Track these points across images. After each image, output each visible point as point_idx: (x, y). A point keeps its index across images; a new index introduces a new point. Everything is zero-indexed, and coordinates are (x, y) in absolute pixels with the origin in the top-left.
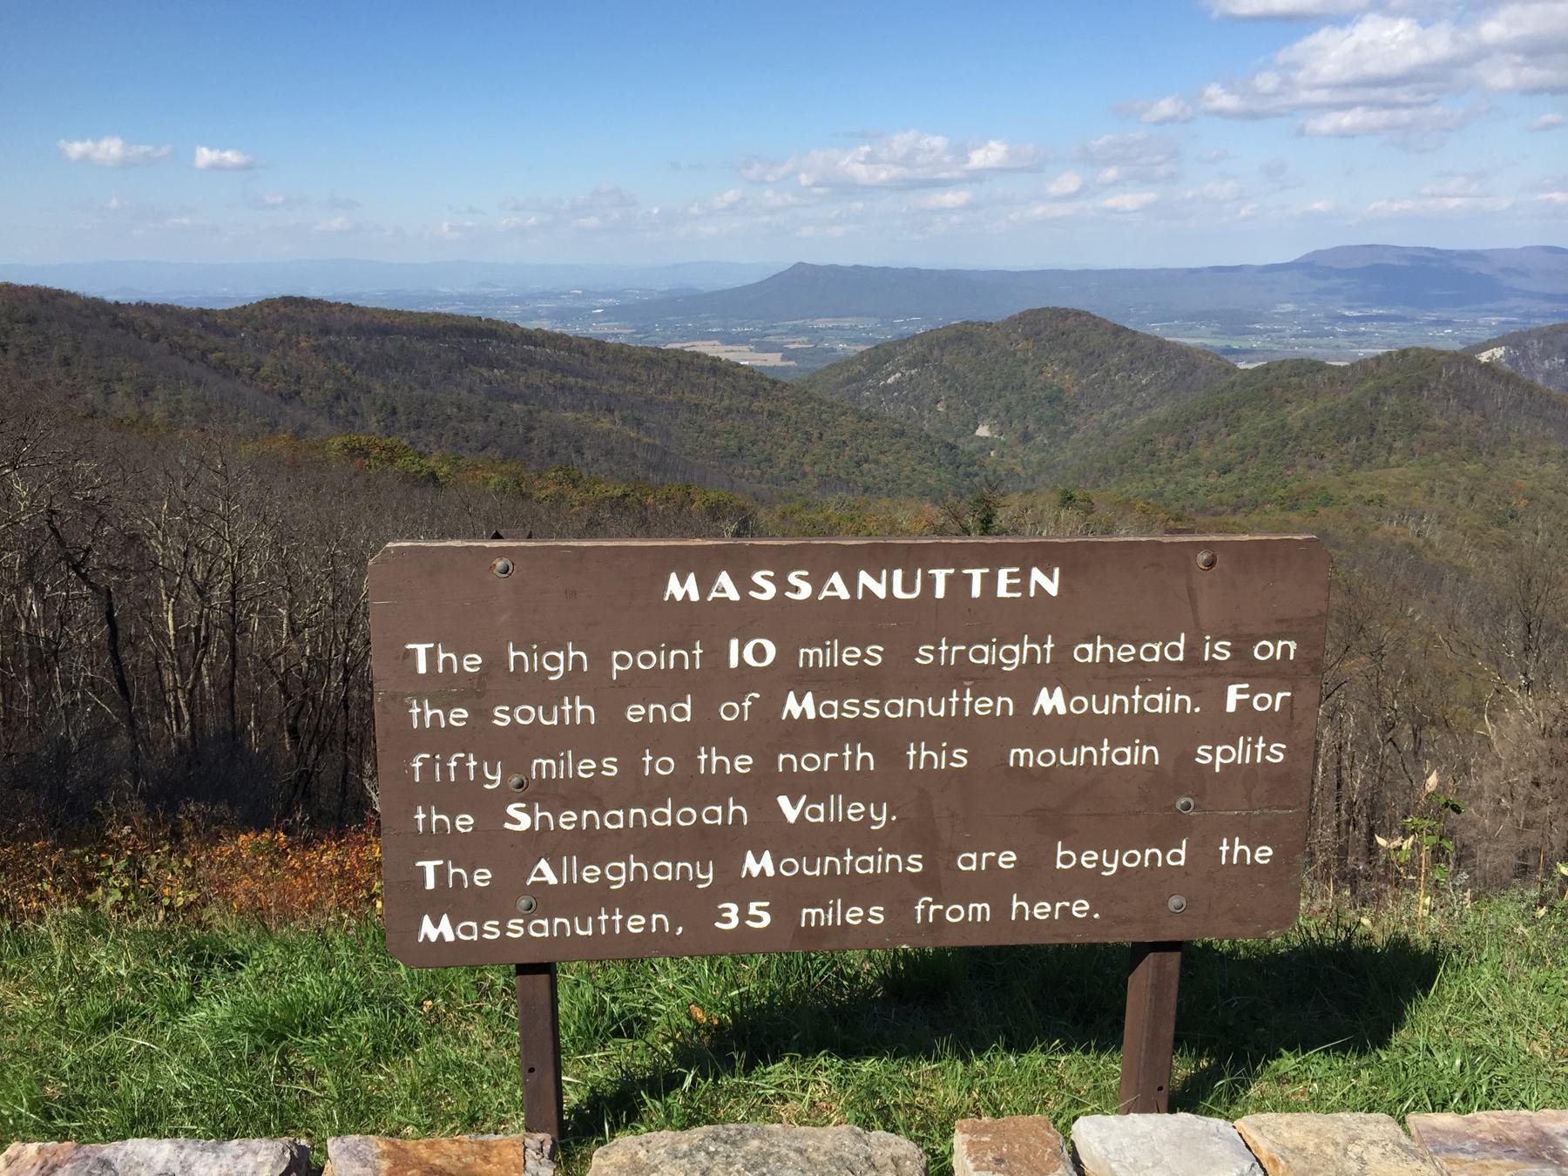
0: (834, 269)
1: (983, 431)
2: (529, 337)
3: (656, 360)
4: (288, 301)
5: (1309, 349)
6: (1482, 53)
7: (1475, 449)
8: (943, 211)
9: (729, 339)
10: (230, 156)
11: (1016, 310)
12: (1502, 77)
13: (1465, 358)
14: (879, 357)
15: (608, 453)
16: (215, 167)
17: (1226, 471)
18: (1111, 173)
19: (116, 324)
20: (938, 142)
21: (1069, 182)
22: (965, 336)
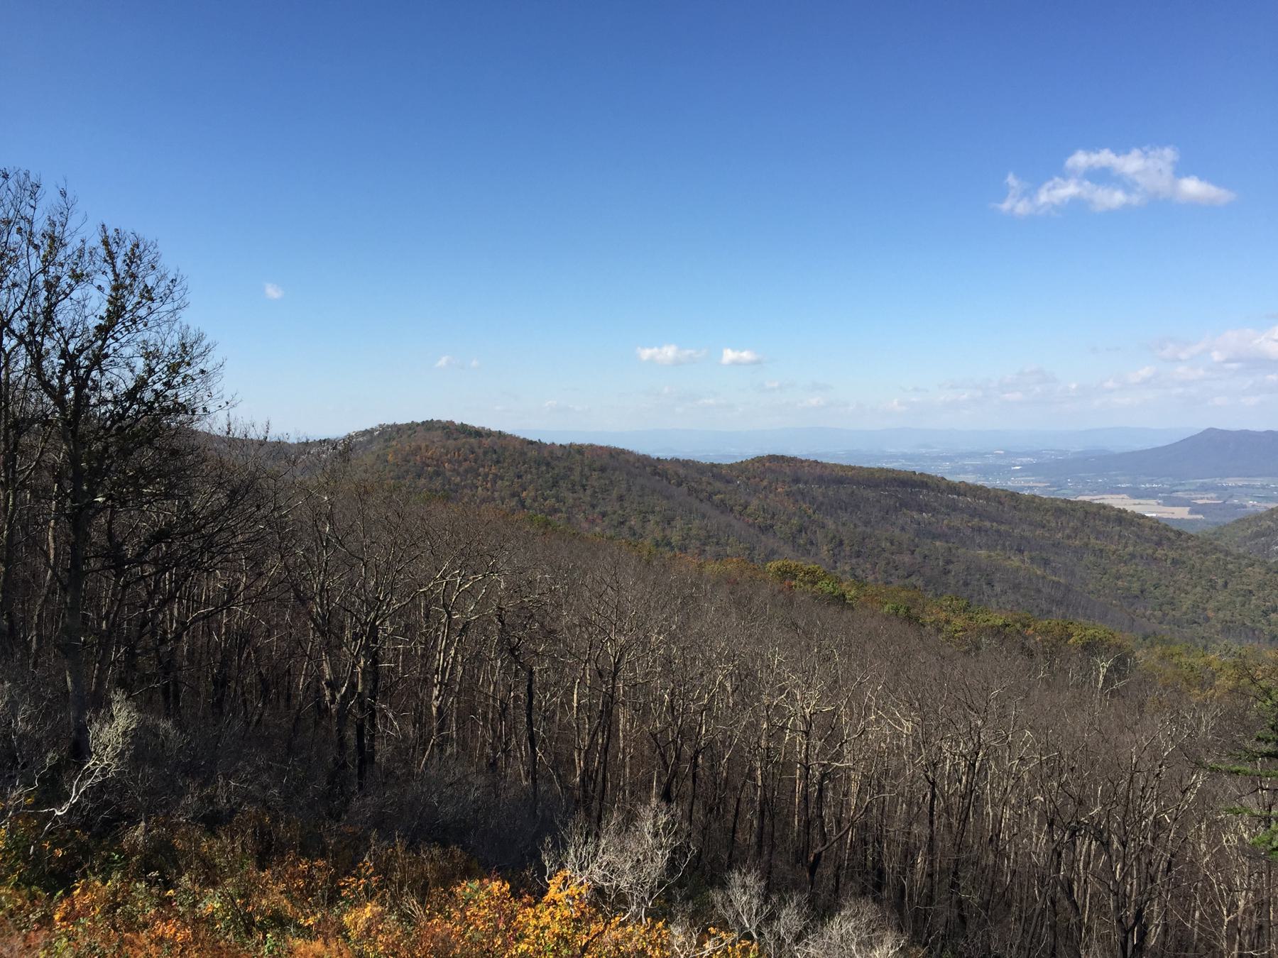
2: (954, 488)
4: (773, 458)
9: (1136, 494)
10: (746, 355)
15: (1016, 587)
16: (735, 363)
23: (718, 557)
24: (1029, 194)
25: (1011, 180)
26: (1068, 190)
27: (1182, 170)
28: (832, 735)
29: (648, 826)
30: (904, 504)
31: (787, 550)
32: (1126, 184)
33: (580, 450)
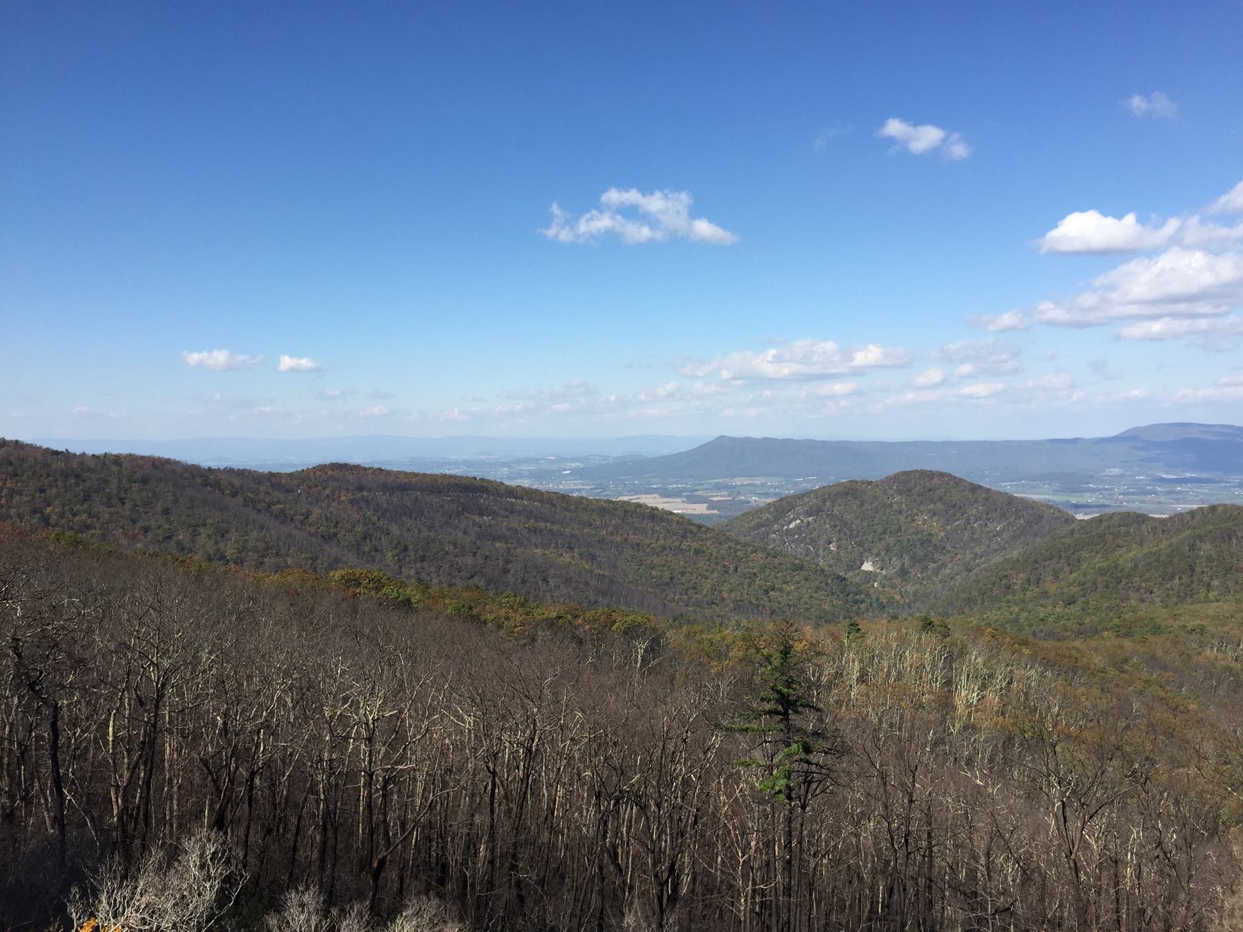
0: (748, 441)
1: (867, 566)
2: (512, 492)
3: (608, 509)
4: (335, 466)
5: (1135, 505)
8: (833, 397)
9: (666, 493)
10: (305, 362)
14: (783, 507)
15: (568, 581)
16: (294, 370)
17: (1070, 602)
18: (966, 368)
19: (216, 485)
20: (830, 345)
22: (851, 492)
23: (277, 569)
24: (571, 223)
25: (555, 209)
26: (604, 222)
27: (695, 212)
28: (396, 735)
29: (194, 858)
30: (466, 509)
31: (352, 558)
32: (650, 220)
33: (117, 460)
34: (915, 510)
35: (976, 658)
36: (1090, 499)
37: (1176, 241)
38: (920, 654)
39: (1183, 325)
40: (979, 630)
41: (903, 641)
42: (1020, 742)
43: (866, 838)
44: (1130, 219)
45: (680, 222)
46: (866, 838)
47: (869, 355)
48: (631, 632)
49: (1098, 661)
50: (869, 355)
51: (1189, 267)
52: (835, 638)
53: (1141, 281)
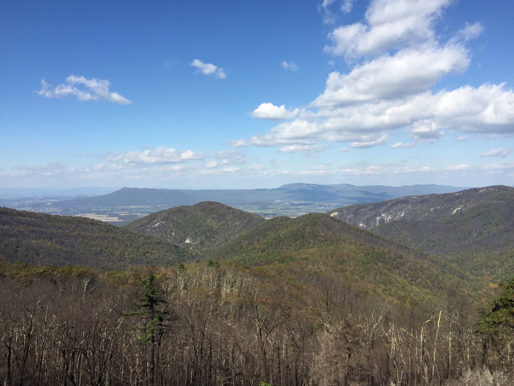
0: (136, 189)
1: (187, 241)
2: (20, 214)
3: (70, 221)
5: (285, 214)
6: (325, 131)
7: (332, 242)
8: (174, 171)
9: (98, 213)
11: (197, 202)
12: (331, 137)
13: (327, 216)
14: (152, 218)
17: (263, 251)
18: (225, 161)
20: (172, 150)
21: (214, 163)
22: (181, 210)
25: (43, 82)
26: (68, 90)
27: (112, 90)
34: (206, 218)
35: (229, 275)
36: (270, 212)
37: (297, 117)
38: (208, 275)
39: (300, 147)
40: (230, 264)
41: (202, 271)
42: (246, 306)
43: (186, 353)
44: (283, 107)
45: (105, 93)
46: (186, 353)
47: (188, 154)
48: (81, 276)
49: (273, 273)
50: (188, 154)
51: (302, 126)
52: (174, 271)
53: (287, 131)
